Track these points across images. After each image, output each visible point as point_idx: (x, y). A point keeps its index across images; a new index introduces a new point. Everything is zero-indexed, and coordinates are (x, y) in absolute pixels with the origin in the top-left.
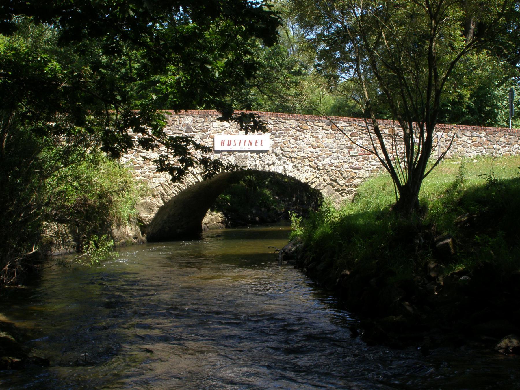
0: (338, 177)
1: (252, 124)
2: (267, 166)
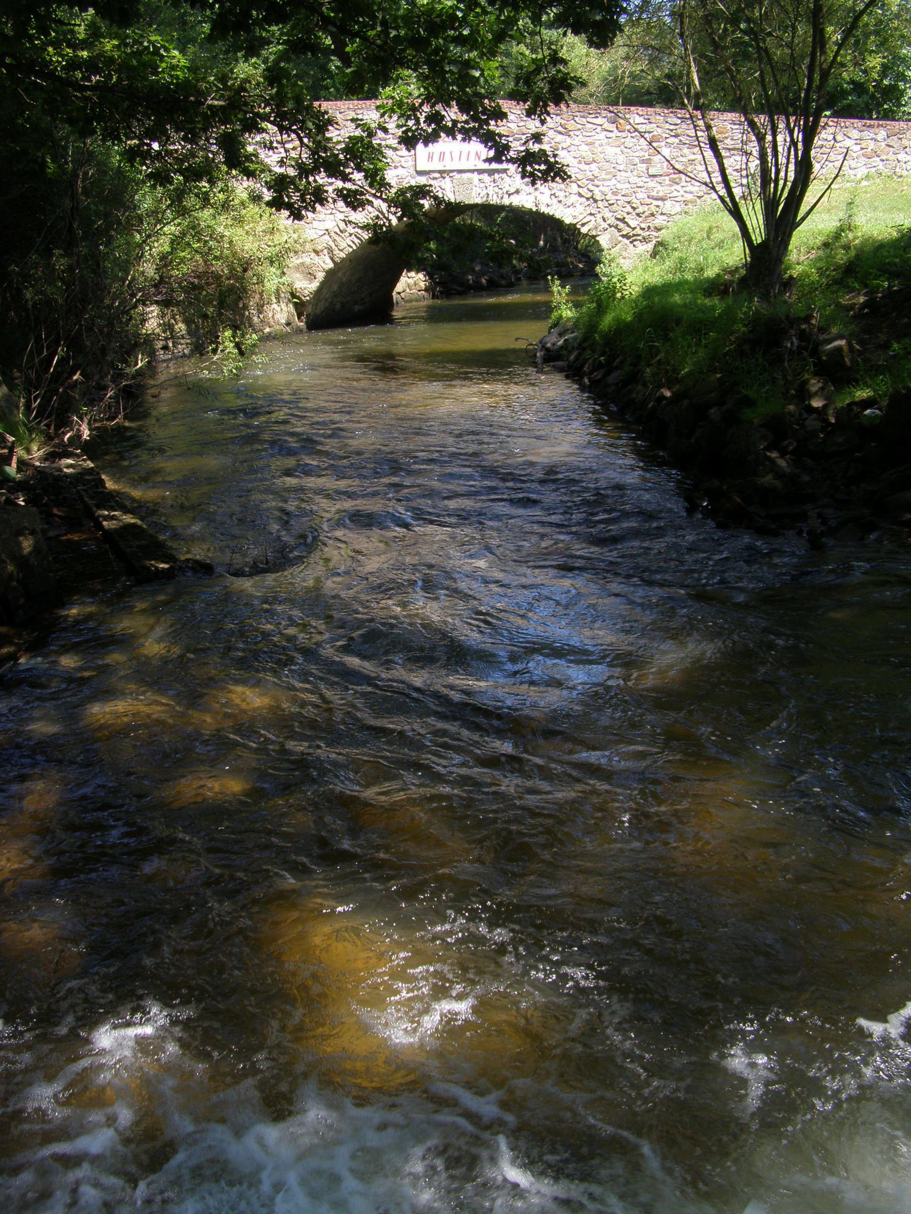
0: (628, 213)
1: (543, 167)
2: (506, 196)
